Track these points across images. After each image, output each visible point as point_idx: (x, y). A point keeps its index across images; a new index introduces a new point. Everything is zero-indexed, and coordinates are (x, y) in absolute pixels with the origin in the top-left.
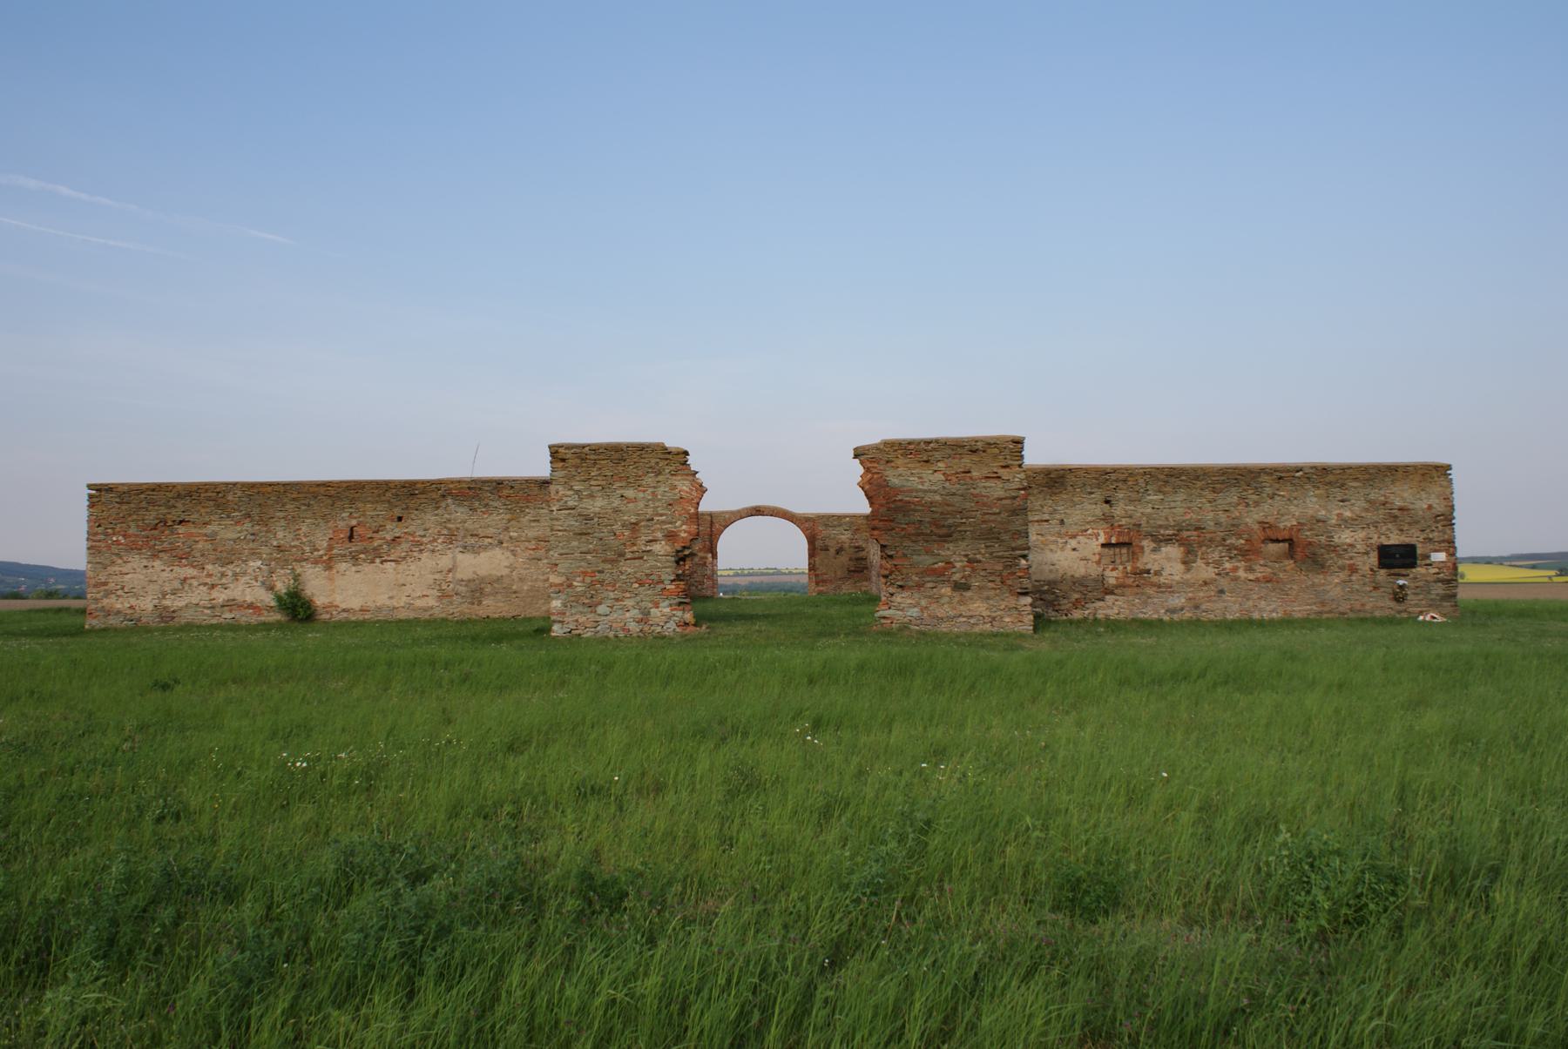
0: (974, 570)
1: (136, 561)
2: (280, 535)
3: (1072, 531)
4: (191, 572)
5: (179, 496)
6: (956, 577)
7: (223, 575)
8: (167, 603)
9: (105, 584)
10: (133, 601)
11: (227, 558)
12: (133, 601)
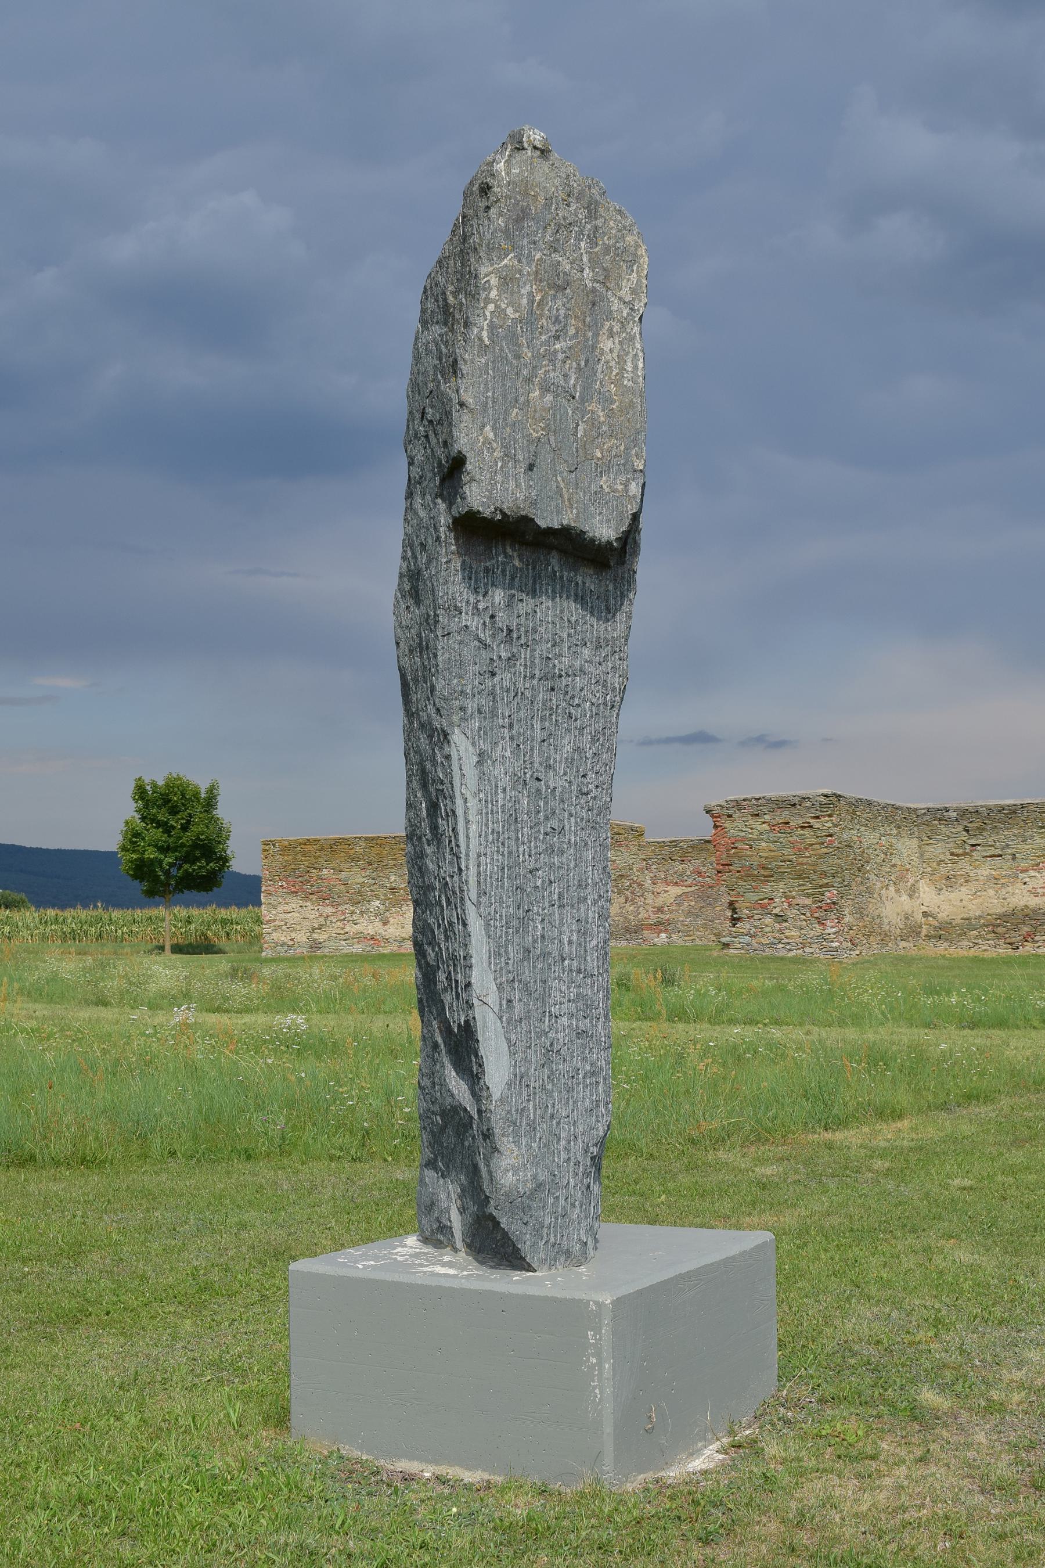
0: (790, 905)
1: (294, 903)
2: (393, 878)
3: (1023, 865)
4: (330, 910)
5: (322, 849)
6: (776, 911)
7: (353, 913)
8: (315, 935)
9: (274, 920)
10: (293, 935)
11: (359, 899)
12: (293, 935)
